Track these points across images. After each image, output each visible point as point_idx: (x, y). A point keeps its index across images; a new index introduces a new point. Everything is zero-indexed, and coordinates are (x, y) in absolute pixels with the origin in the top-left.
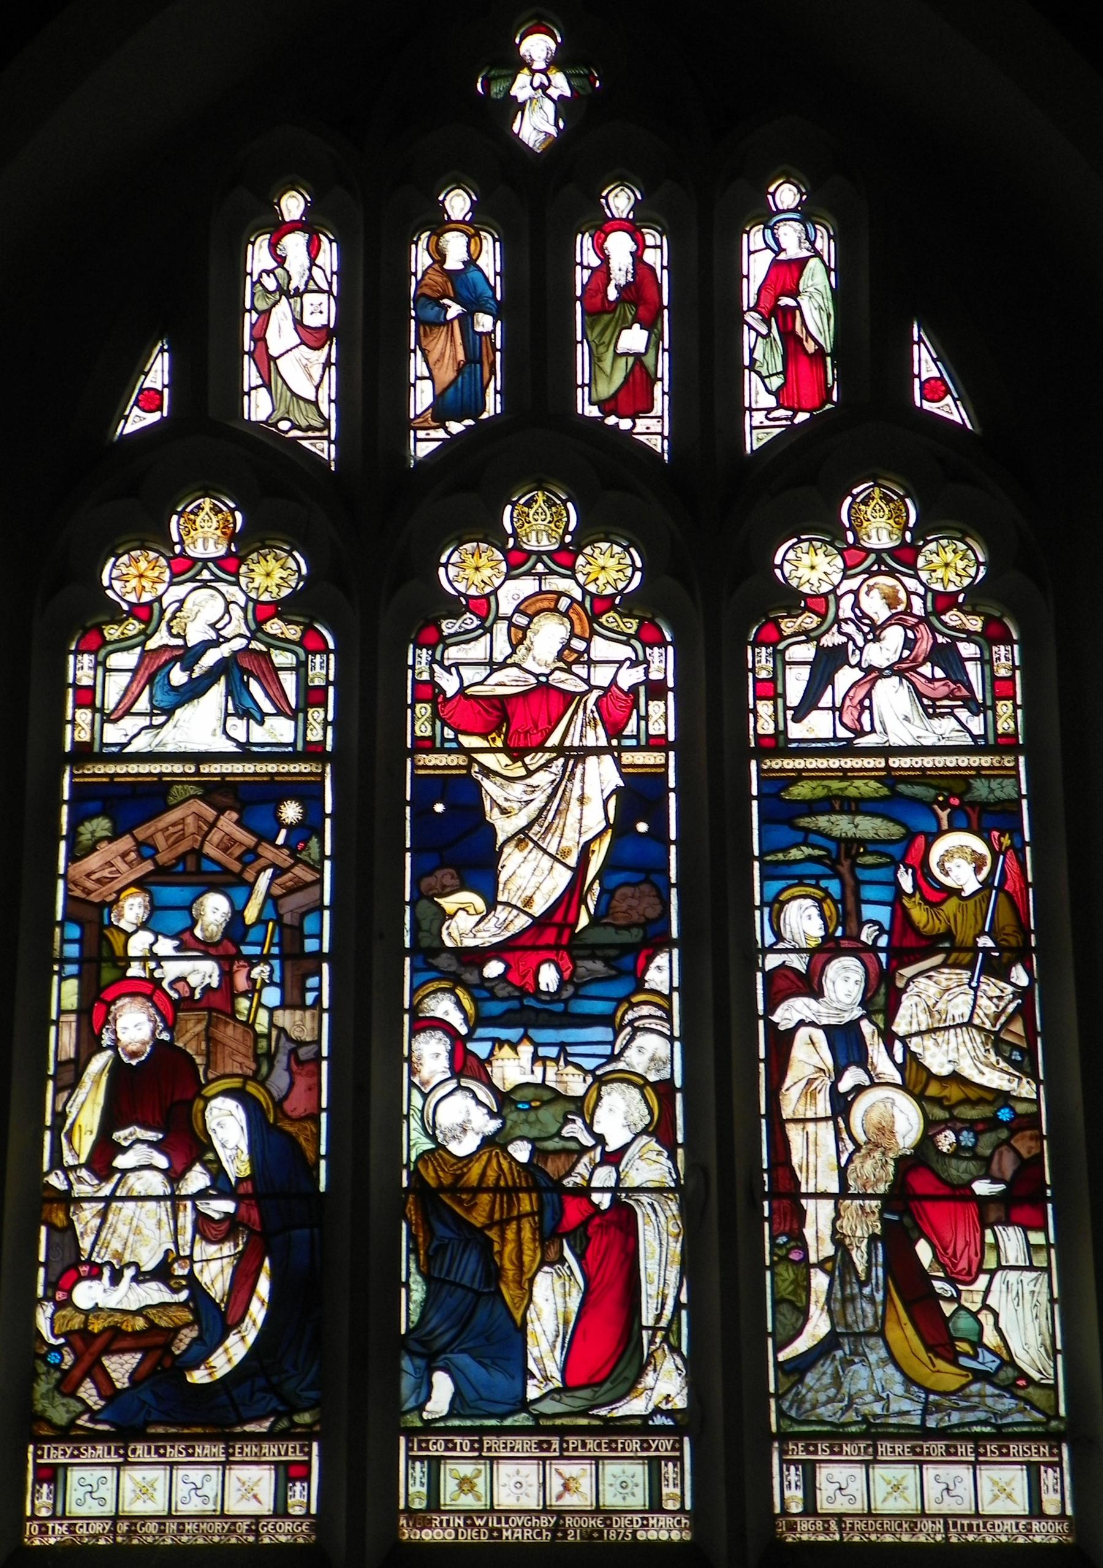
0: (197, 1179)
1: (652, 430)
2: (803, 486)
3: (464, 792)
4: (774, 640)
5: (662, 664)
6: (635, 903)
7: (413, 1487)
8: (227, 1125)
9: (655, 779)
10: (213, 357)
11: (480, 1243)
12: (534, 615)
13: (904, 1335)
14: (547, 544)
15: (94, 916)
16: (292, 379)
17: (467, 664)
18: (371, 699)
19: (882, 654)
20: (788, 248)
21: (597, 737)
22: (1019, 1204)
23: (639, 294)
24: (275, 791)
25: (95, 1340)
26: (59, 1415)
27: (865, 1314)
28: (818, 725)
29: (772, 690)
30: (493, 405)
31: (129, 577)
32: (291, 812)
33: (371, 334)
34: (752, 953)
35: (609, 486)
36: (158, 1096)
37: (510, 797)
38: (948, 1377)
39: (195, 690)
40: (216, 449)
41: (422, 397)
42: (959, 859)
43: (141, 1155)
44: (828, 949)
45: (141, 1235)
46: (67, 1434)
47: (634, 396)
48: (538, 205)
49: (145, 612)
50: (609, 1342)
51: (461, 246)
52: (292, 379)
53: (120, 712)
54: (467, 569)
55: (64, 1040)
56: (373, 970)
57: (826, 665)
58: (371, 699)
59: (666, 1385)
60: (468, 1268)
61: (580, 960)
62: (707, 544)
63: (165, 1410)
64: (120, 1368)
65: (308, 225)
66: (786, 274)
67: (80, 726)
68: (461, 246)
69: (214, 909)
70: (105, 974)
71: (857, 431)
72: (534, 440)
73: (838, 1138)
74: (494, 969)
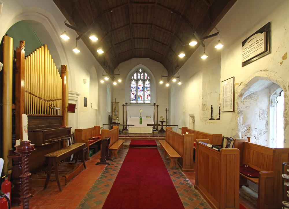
1: (143, 79)
10: (134, 77)
12: (140, 83)
16: (135, 78)
18: (137, 85)
20: (146, 74)
35: (142, 80)
36: (133, 94)
37: (140, 87)
40: (134, 79)
42: (149, 89)
43: (133, 95)
45: (133, 97)
47: (142, 78)
48: (141, 73)
51: (139, 74)
52: (135, 78)
53: (132, 85)
56: (137, 91)
58: (137, 85)
62: (144, 81)
63: (133, 100)
68: (139, 74)
69: (134, 90)
71: (147, 79)
73: (146, 95)
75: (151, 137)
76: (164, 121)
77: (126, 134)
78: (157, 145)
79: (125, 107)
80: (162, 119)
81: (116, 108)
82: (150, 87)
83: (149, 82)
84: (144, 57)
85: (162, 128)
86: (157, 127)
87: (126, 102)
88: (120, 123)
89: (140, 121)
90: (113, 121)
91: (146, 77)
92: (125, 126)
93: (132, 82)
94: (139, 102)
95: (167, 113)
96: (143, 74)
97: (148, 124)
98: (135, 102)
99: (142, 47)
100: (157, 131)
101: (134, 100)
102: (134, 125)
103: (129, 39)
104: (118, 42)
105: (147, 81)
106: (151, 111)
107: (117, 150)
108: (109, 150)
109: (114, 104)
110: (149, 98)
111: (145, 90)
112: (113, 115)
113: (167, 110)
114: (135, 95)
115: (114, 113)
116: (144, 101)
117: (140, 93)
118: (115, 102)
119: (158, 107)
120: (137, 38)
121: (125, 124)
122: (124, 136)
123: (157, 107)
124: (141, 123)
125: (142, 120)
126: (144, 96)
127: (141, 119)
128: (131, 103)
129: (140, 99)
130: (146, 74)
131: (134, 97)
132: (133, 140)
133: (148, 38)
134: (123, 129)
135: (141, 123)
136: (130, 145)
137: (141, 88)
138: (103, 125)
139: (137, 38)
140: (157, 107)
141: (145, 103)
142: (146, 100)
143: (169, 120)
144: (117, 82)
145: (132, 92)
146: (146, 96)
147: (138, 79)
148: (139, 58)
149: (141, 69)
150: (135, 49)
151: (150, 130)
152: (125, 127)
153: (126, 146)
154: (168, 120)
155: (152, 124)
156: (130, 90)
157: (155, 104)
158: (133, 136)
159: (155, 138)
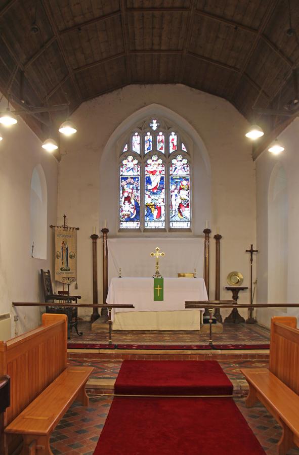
0: (131, 205)
1: (163, 151)
2: (174, 155)
3: (149, 178)
4: (171, 167)
5: (164, 169)
6: (161, 186)
7: (146, 225)
8: (133, 201)
9: (163, 177)
11: (150, 209)
12: (154, 164)
13: (179, 215)
14: (213, 331)
15: (123, 187)
16: (136, 148)
17: (149, 169)
18: (143, 171)
19: (180, 167)
20: (173, 137)
21: (159, 174)
22: (188, 206)
23: (162, 141)
24: (136, 178)
25: (124, 216)
26: (122, 220)
27: (177, 214)
28: (175, 173)
29: (171, 171)
30: (151, 149)
31: (124, 162)
32: (137, 179)
33: (142, 144)
34: (170, 189)
35: (160, 156)
36: (128, 199)
37: (152, 178)
38: (182, 218)
39: (130, 170)
40: (130, 152)
41: (146, 149)
42: (184, 183)
43: (126, 202)
44: (175, 189)
45: (127, 209)
46: (122, 221)
47: (162, 148)
48: (155, 134)
49: (126, 165)
50: (159, 215)
51: (149, 137)
52: (136, 148)
53: (125, 172)
54: (149, 161)
55: (121, 195)
56: (143, 191)
57: (176, 168)
58: (143, 171)
59: (163, 218)
60: (150, 211)
61: (158, 189)
62: (167, 159)
63: (129, 219)
64: (126, 217)
65: (137, 136)
66: (173, 140)
67: (121, 173)
68: (149, 137)
69: (131, 186)
70: (124, 191)
71: (178, 151)
72: (154, 151)
73: (175, 203)
74: (151, 190)
75: (200, 348)
76: (243, 289)
77: (101, 336)
78: (231, 387)
79: (99, 241)
80: (233, 281)
81: (69, 246)
82: (189, 177)
83: (185, 161)
84: (166, 82)
85: (235, 314)
86: (217, 311)
87: (105, 227)
88: (80, 297)
89: (155, 291)
90: (56, 290)
91: (175, 144)
92: (100, 310)
93: (124, 162)
94: (151, 225)
95: (252, 260)
96: (163, 137)
97: (187, 303)
98: (133, 225)
99: (160, 44)
100: (219, 324)
101: (132, 220)
102: (132, 306)
103: (114, 13)
104: (70, 24)
105: (179, 158)
106: (194, 253)
107: (44, 435)
108: (5, 436)
109: (61, 236)
110: (187, 212)
111: (173, 187)
112: (58, 270)
113: (251, 251)
114: (136, 202)
115: (59, 263)
116: (168, 221)
117: (153, 197)
118: (65, 227)
119: (221, 241)
120: (141, 9)
121: (100, 302)
122: (92, 347)
123: (218, 244)
124: (159, 296)
125: (162, 286)
126: (169, 206)
127: (159, 283)
128: (121, 230)
129: (152, 216)
130: (175, 137)
131: (132, 211)
132: (130, 367)
133: (183, 8)
134: (95, 317)
135: (159, 296)
136: (117, 389)
137: (155, 180)
138: (15, 304)
139: (141, 9)
140: (218, 244)
141: (171, 230)
142: (177, 218)
143: (259, 284)
144: (58, 139)
145: (126, 195)
146: (175, 207)
147: (146, 152)
148: (148, 86)
149: (155, 121)
150: (135, 51)
151: (193, 320)
152: (102, 313)
153: (98, 390)
154: (256, 283)
155: (205, 302)
156: (118, 188)
157: (207, 232)
158: (130, 347)
159: (219, 352)
